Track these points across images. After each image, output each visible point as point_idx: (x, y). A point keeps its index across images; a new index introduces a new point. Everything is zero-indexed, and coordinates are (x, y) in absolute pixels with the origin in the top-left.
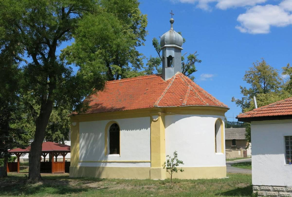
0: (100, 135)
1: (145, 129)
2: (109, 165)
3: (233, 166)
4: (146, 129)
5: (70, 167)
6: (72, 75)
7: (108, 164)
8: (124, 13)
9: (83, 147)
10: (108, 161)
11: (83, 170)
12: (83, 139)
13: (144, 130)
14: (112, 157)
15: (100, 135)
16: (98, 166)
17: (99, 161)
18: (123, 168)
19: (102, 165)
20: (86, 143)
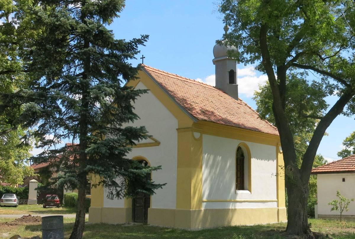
0: (228, 164)
1: (254, 158)
2: (238, 206)
3: (126, 175)
4: (255, 158)
5: (149, 208)
6: (309, 86)
7: (238, 204)
8: (0, 3)
9: (206, 180)
10: (238, 200)
11: (209, 218)
12: (205, 167)
13: (271, 162)
14: (242, 194)
15: (228, 164)
16: (228, 208)
17: (228, 200)
18: (255, 210)
19: (231, 207)
20: (210, 173)
